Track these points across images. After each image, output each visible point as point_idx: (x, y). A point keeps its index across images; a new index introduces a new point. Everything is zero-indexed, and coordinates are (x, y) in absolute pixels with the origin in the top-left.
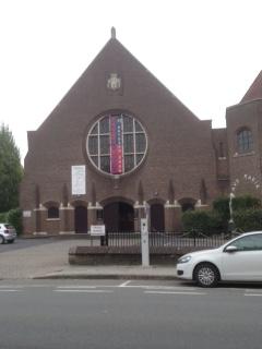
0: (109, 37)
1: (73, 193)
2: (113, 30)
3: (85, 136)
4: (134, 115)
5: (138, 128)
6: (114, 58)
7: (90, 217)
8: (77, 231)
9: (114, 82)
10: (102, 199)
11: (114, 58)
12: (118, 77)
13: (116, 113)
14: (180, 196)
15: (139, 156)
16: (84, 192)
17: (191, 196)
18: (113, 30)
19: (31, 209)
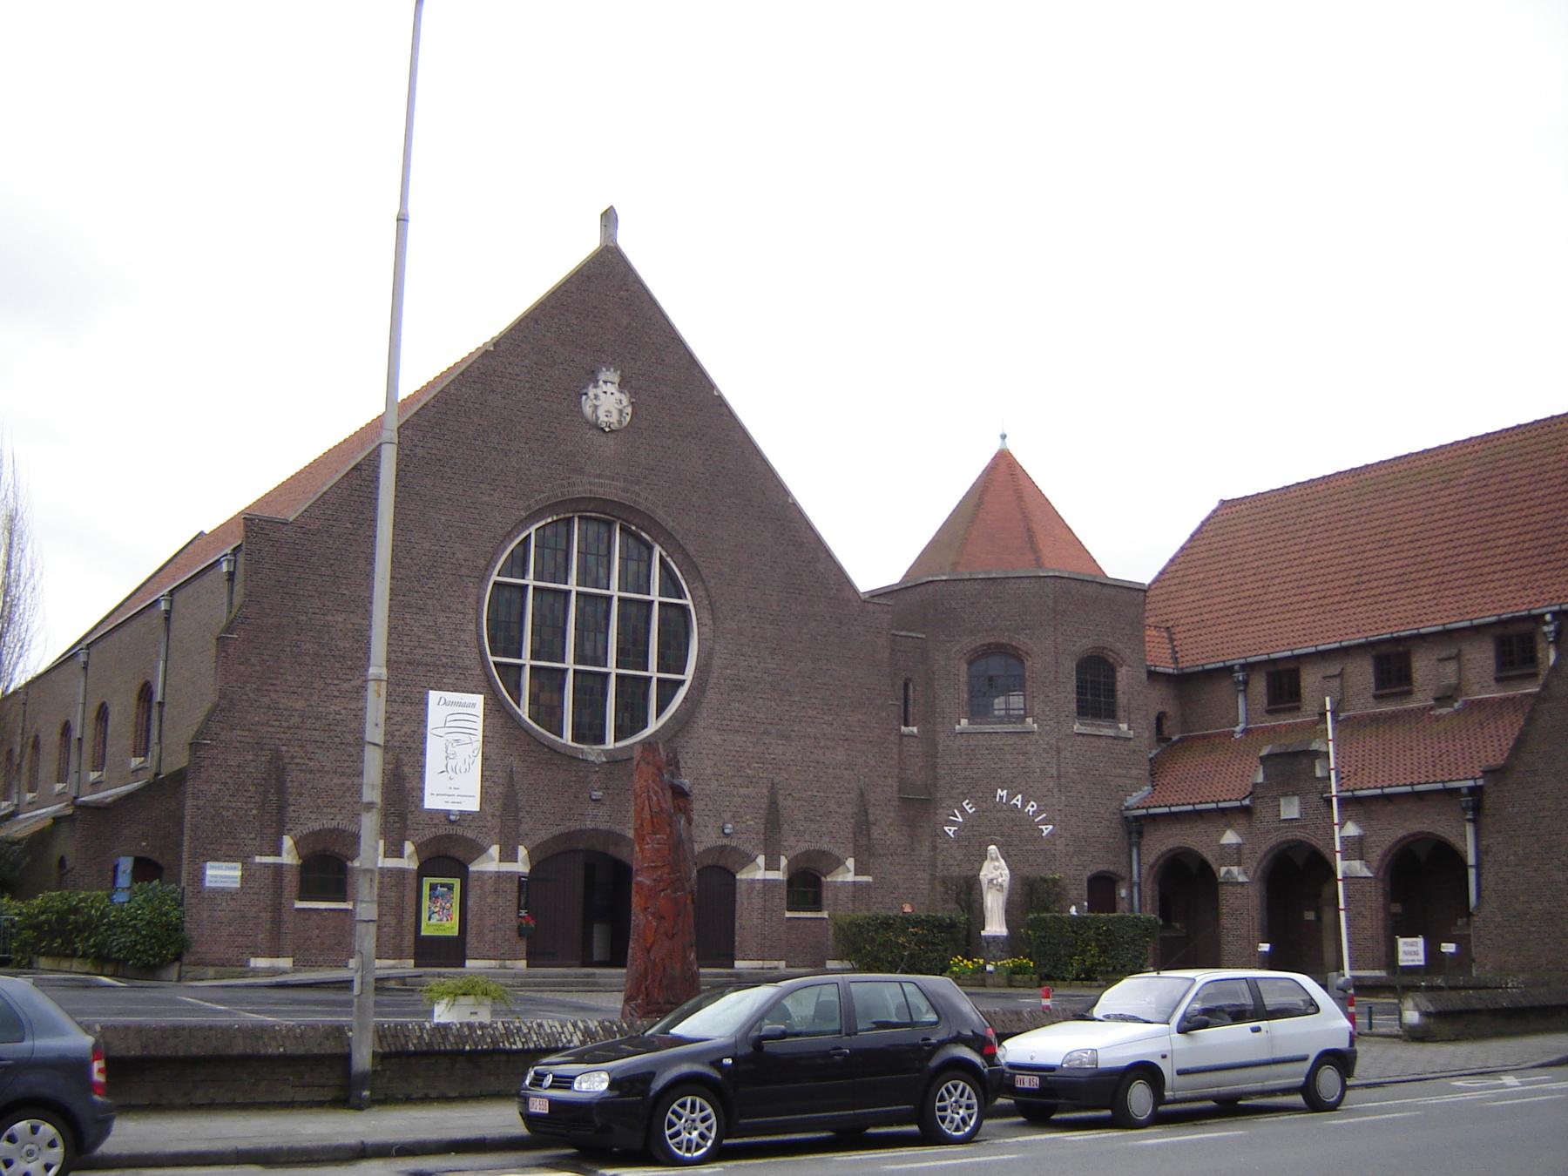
0: (587, 244)
1: (431, 802)
2: (609, 218)
3: (483, 579)
4: (667, 539)
5: (670, 585)
6: (602, 311)
7: (748, 916)
8: (534, 958)
9: (607, 401)
10: (543, 835)
11: (602, 311)
12: (622, 386)
13: (602, 514)
14: (795, 844)
15: (667, 690)
16: (473, 805)
17: (825, 845)
18: (609, 218)
19: (244, 859)
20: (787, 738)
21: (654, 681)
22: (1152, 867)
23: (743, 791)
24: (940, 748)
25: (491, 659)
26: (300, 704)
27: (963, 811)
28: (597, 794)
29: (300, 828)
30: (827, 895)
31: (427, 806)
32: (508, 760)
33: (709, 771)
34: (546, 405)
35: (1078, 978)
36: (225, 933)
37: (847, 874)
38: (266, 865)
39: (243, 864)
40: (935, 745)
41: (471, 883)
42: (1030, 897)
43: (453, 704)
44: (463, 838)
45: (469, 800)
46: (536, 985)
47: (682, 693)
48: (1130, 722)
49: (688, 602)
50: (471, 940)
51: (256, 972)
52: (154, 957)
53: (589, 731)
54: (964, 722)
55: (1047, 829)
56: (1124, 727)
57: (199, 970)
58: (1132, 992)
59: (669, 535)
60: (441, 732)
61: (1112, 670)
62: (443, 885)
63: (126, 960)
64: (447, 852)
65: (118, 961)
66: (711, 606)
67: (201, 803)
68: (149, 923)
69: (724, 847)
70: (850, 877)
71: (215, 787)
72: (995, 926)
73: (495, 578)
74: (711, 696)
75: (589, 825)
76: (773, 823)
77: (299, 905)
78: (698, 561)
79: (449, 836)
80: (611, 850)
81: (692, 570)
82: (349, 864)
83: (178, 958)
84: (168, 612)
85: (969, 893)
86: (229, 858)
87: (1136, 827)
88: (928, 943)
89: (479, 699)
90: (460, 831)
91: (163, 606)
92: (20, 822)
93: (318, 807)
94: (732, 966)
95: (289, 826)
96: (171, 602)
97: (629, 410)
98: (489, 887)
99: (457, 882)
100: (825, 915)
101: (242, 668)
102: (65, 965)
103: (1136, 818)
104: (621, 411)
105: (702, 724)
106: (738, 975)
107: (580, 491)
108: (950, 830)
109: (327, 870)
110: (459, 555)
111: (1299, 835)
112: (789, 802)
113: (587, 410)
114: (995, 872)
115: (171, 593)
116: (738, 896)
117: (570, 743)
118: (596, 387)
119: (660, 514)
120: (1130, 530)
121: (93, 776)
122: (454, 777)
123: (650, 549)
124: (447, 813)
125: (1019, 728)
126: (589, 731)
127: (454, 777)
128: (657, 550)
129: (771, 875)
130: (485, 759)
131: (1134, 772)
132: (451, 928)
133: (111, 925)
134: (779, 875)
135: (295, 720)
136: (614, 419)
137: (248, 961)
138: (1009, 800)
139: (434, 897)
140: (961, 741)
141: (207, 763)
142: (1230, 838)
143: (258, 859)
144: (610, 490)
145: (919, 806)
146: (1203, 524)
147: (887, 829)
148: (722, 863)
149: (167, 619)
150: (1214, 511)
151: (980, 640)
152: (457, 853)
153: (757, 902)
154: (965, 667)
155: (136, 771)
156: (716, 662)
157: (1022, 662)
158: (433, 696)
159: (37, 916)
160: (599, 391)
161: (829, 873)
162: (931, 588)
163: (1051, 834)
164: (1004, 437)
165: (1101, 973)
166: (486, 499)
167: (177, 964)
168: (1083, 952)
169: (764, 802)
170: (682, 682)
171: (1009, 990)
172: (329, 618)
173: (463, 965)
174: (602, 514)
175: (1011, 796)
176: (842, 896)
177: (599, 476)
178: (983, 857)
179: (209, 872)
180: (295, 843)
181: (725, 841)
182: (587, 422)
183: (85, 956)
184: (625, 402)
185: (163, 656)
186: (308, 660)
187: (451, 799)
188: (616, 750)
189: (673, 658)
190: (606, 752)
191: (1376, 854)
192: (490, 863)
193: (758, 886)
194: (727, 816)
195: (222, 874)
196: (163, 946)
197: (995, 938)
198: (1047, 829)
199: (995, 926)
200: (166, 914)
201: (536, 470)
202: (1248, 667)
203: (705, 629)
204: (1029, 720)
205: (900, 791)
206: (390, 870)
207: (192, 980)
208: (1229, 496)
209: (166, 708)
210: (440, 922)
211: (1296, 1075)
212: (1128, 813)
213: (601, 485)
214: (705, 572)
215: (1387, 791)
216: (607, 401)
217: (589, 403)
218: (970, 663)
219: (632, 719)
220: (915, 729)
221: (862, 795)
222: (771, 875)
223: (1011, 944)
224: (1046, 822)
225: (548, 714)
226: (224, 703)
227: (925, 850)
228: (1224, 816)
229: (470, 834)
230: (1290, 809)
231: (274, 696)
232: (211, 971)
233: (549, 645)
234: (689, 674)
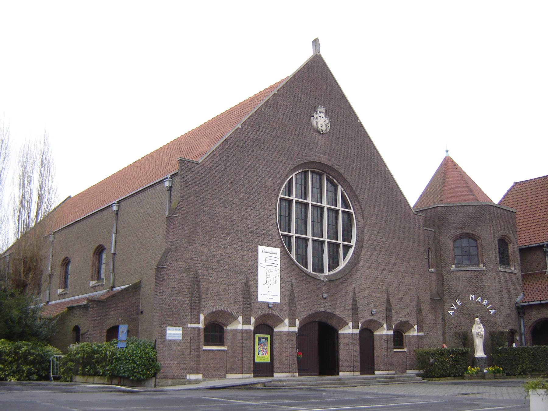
0: (307, 55)
1: (261, 298)
2: (316, 42)
5: (345, 204)
6: (314, 82)
10: (305, 314)
11: (314, 82)
12: (327, 114)
14: (397, 319)
15: (347, 248)
16: (278, 300)
17: (407, 319)
18: (316, 42)
19: (183, 325)
20: (392, 272)
21: (341, 245)
22: (530, 327)
23: (378, 295)
24: (444, 277)
25: (280, 232)
26: (206, 250)
27: (456, 304)
28: (325, 295)
29: (207, 310)
30: (406, 341)
31: (259, 300)
32: (291, 279)
33: (365, 286)
34: (298, 120)
35: (520, 374)
36: (175, 362)
37: (414, 332)
38: (194, 328)
39: (183, 328)
40: (442, 276)
41: (275, 337)
42: (493, 341)
43: (268, 252)
44: (274, 315)
46: (328, 384)
47: (351, 251)
48: (515, 267)
49: (352, 211)
50: (276, 364)
51: (190, 382)
52: (143, 375)
53: (318, 268)
54: (453, 266)
55: (492, 311)
56: (513, 269)
57: (164, 381)
59: (346, 181)
60: (264, 265)
61: (507, 245)
62: (263, 338)
63: (128, 377)
65: (123, 377)
66: (362, 213)
67: (164, 297)
68: (140, 358)
69: (372, 320)
70: (416, 333)
71: (170, 289)
72: (480, 353)
73: (280, 196)
74: (364, 253)
75: (323, 310)
76: (355, 311)
77: (205, 348)
78: (357, 193)
79: (268, 315)
80: (329, 322)
81: (354, 196)
82: (225, 328)
83: (155, 375)
84: (117, 211)
85: (466, 339)
86: (177, 325)
87: (521, 310)
88: (456, 361)
89: (278, 250)
90: (272, 312)
91: (115, 208)
93: (214, 299)
94: (374, 374)
95: (202, 309)
96: (119, 206)
97: (329, 125)
98: (284, 339)
99: (269, 336)
100: (405, 350)
101: (180, 231)
102: (91, 379)
103: (522, 306)
104: (326, 125)
105: (361, 264)
106: (340, 379)
107: (312, 159)
108: (451, 313)
109: (215, 332)
110: (268, 184)
112: (394, 300)
113: (314, 123)
114: (478, 330)
115: (119, 202)
116: (375, 342)
117: (312, 272)
118: (316, 114)
119: (342, 171)
121: (60, 291)
122: (269, 288)
124: (268, 304)
125: (477, 268)
126: (318, 268)
127: (269, 288)
128: (340, 188)
129: (246, 327)
130: (281, 278)
131: (518, 287)
132: (267, 358)
133: (118, 359)
135: (204, 258)
136: (324, 128)
137: (186, 376)
138: (475, 299)
139: (260, 344)
140: (453, 274)
141: (166, 277)
143: (189, 325)
144: (324, 159)
145: (439, 301)
146: (508, 191)
147: (427, 314)
148: (369, 327)
149: (117, 214)
150: (513, 186)
151: (459, 232)
152: (269, 323)
153: (384, 345)
154: (452, 243)
155: (60, 295)
156: (366, 238)
157: (476, 241)
158: (260, 248)
159: (75, 355)
160: (318, 116)
161: (407, 331)
162: (437, 209)
163: (494, 313)
164: (447, 151)
165: (530, 372)
166: (277, 159)
167: (154, 378)
168: (523, 363)
169: (385, 300)
170: (351, 246)
171: (496, 380)
172: (217, 209)
174: (321, 170)
175: (476, 297)
176: (412, 342)
177: (319, 153)
178: (473, 323)
179: (168, 332)
180: (205, 317)
181: (372, 317)
182: (314, 129)
183: (104, 375)
184: (327, 122)
185: (114, 230)
186: (208, 229)
187: (269, 297)
188: (329, 275)
189: (347, 237)
190: (326, 276)
192: (285, 327)
193: (384, 337)
194: (372, 306)
195: (174, 333)
196: (148, 369)
197: (481, 358)
198: (492, 311)
199: (480, 353)
200: (148, 353)
201: (295, 148)
203: (360, 223)
204: (481, 265)
205: (431, 296)
206: (246, 330)
207: (161, 386)
208: (518, 180)
209: (117, 256)
210: (263, 356)
212: (518, 305)
213: (320, 157)
214: (359, 198)
215: (542, 302)
216: (321, 121)
217: (315, 120)
218: (454, 241)
219: (334, 264)
220: (433, 270)
221: (418, 297)
222: (246, 327)
223: (490, 361)
224: (491, 308)
225: (303, 258)
226: (173, 248)
227: (440, 322)
229: (277, 314)
231: (195, 245)
232: (170, 382)
233: (302, 228)
234: (353, 242)
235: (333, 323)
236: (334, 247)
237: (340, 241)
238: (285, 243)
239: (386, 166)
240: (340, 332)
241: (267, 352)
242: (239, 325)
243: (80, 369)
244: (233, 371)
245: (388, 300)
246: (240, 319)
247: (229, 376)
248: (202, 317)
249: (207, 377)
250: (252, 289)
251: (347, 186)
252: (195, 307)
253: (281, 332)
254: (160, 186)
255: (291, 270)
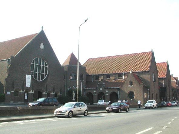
0: (41, 30)
1: (26, 86)
2: (43, 27)
5: (46, 65)
6: (41, 38)
9: (42, 46)
11: (41, 38)
12: (43, 45)
15: (46, 75)
16: (30, 86)
18: (43, 27)
19: (10, 91)
45: (29, 86)
47: (46, 76)
53: (39, 79)
58: (68, 104)
64: (27, 90)
89: (30, 76)
92: (93, 104)
99: (27, 94)
111: (102, 91)
120: (82, 61)
122: (28, 84)
123: (44, 61)
126: (39, 79)
127: (28, 84)
129: (23, 92)
134: (46, 93)
142: (95, 91)
152: (28, 91)
156: (50, 73)
158: (27, 75)
173: (28, 102)
189: (46, 73)
191: (109, 93)
195: (8, 93)
202: (94, 75)
211: (83, 112)
216: (42, 46)
219: (42, 78)
222: (23, 92)
225: (36, 77)
228: (94, 90)
230: (101, 89)
233: (36, 71)
234: (47, 74)
235: (41, 91)
236: (43, 75)
237: (44, 73)
238: (32, 74)
239: (56, 56)
240: (43, 93)
241: (74, 107)
242: (21, 91)
243: (128, 101)
244: (20, 101)
245: (54, 87)
246: (22, 90)
247: (19, 102)
248: (14, 90)
249: (14, 102)
250: (24, 83)
251: (47, 61)
252: (13, 87)
253: (30, 93)
254: (5, 61)
255: (32, 80)
